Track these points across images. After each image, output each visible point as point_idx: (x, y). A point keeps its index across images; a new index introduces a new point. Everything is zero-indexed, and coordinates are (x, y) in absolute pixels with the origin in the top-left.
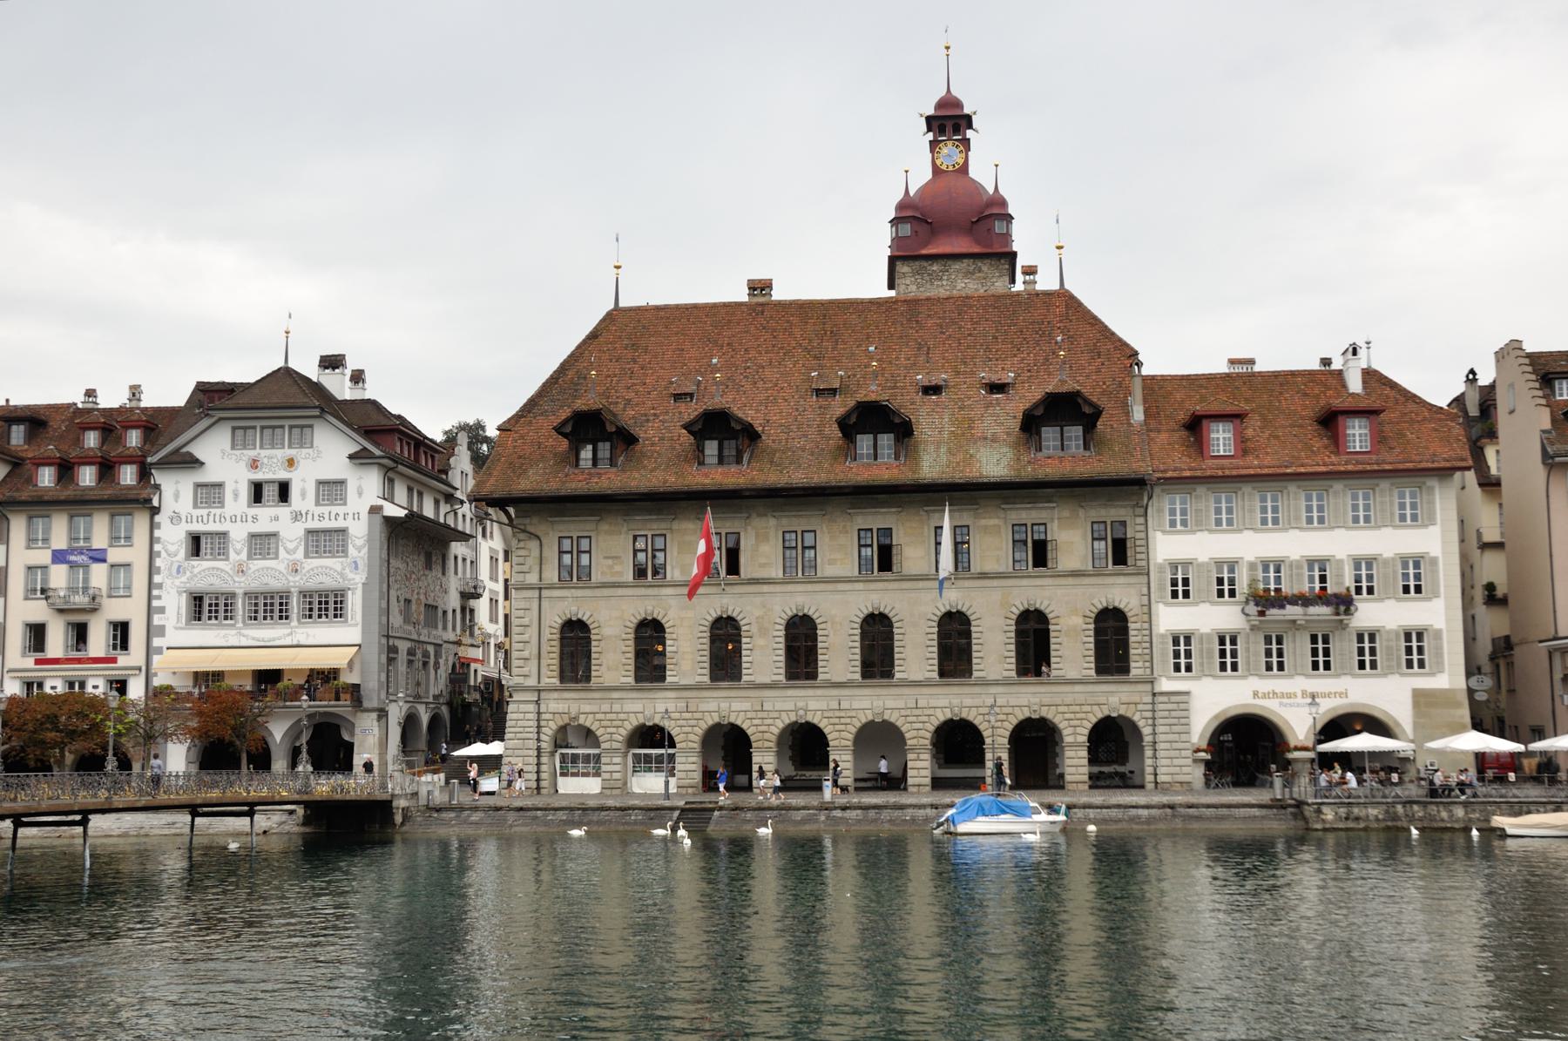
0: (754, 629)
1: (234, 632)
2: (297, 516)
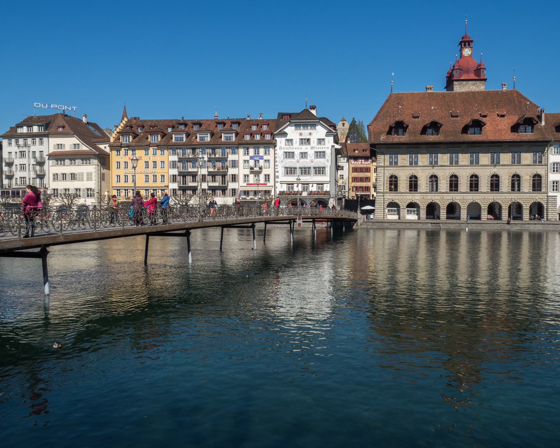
0: (441, 178)
2: (312, 148)
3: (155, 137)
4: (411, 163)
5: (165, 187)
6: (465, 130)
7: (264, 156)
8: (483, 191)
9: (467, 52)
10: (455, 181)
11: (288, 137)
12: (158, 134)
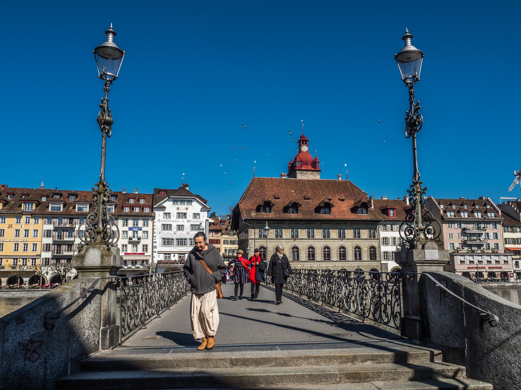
0: (301, 249)
1: (173, 248)
2: (188, 221)
3: (29, 205)
4: (277, 236)
5: (37, 255)
6: (318, 210)
8: (334, 260)
9: (305, 148)
10: (312, 251)
11: (166, 211)
12: (33, 202)
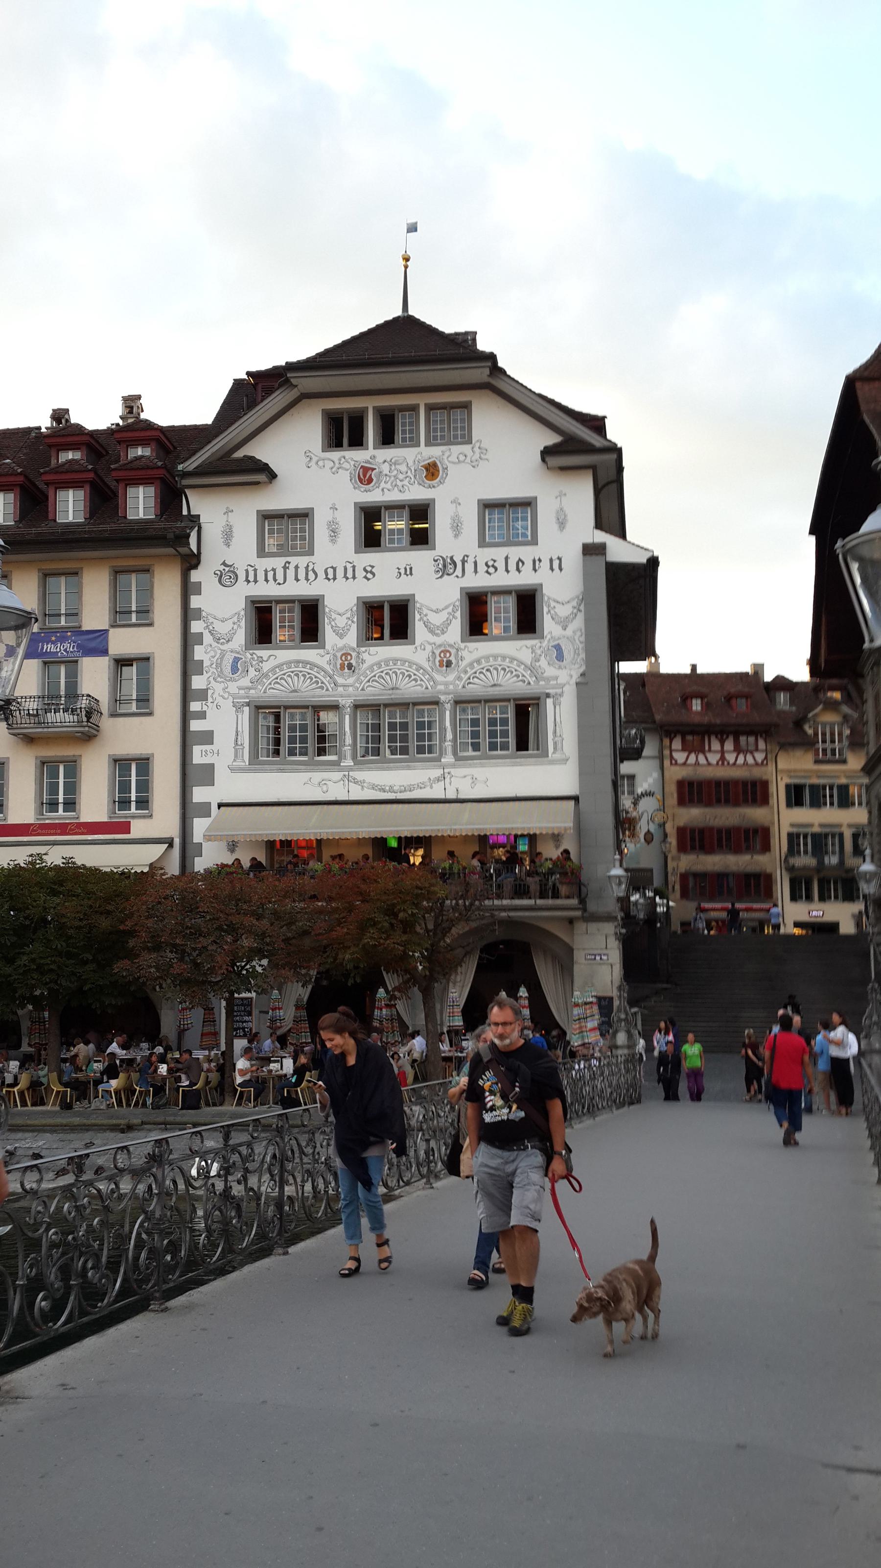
2: (446, 567)
7: (114, 634)
